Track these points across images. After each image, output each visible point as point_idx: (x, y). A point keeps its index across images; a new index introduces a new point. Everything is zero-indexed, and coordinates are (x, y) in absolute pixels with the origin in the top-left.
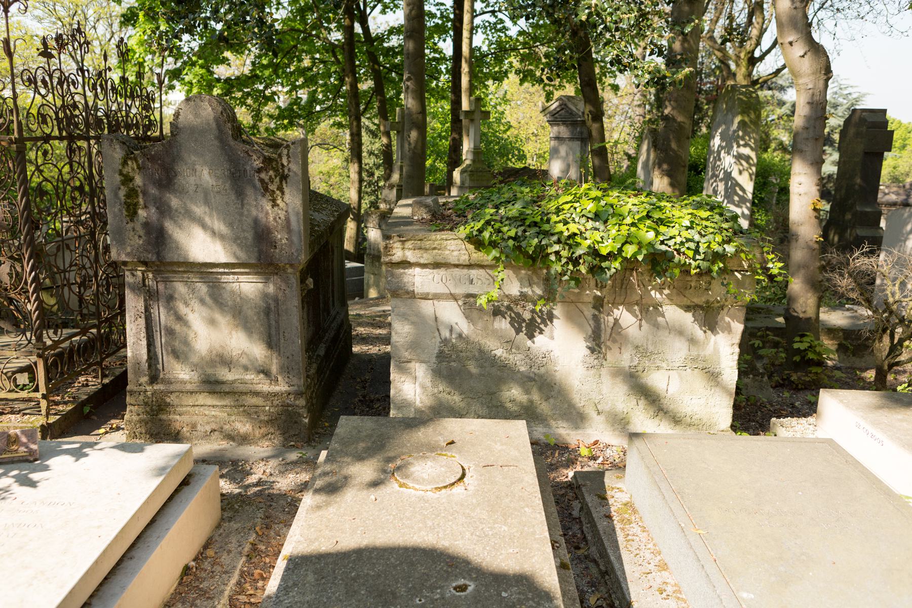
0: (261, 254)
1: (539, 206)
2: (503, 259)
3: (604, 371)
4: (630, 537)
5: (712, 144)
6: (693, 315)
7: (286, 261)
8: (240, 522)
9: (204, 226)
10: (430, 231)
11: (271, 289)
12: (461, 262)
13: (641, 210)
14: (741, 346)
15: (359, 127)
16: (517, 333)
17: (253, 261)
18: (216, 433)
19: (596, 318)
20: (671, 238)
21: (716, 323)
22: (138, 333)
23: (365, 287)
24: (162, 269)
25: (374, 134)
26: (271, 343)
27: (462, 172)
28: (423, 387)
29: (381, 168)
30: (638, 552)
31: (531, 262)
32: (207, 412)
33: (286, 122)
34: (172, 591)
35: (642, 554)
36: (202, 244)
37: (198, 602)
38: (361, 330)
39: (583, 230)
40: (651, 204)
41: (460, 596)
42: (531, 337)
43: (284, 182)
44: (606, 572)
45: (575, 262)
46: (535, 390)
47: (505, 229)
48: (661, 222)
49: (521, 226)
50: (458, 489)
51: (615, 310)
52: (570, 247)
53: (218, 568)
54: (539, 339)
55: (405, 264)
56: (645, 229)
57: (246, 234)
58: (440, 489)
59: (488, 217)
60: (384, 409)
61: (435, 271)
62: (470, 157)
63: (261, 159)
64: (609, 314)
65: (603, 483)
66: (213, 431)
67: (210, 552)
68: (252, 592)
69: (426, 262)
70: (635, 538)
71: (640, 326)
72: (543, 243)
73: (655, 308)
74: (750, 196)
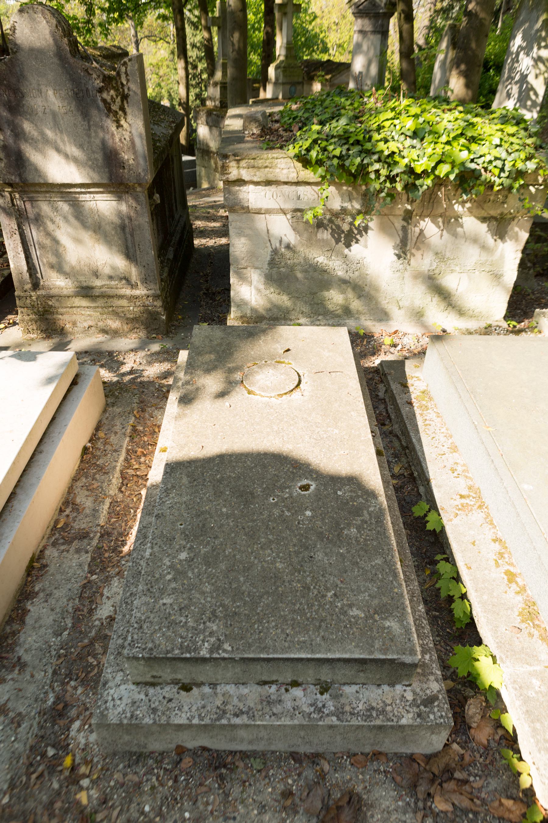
0: (112, 174)
1: (361, 122)
2: (328, 177)
3: (407, 274)
4: (427, 422)
5: (512, 44)
6: (488, 226)
7: (135, 181)
8: (121, 407)
9: (58, 150)
10: (262, 149)
11: (124, 208)
12: (290, 180)
13: (456, 127)
14: (523, 252)
15: (183, 20)
16: (337, 243)
17: (105, 181)
18: (93, 328)
19: (404, 229)
20: (481, 156)
21: (506, 232)
22: (16, 247)
23: (198, 178)
24: (26, 189)
25: (195, 26)
26: (129, 254)
27: (277, 68)
28: (259, 291)
29: (203, 61)
30: (434, 435)
31: (352, 179)
32: (83, 312)
33: (116, 15)
34: (76, 468)
35: (437, 438)
36: (59, 167)
37: (97, 476)
38: (199, 224)
39: (401, 148)
40: (465, 121)
41: (305, 495)
42: (348, 246)
43: (125, 102)
44: (407, 447)
45: (392, 179)
46: (349, 290)
47: (331, 148)
48: (473, 140)
49: (345, 144)
50: (296, 394)
51: (422, 222)
52: (389, 165)
53: (108, 447)
54: (355, 247)
55: (240, 182)
56: (459, 148)
57: (96, 156)
58: (281, 395)
59: (315, 136)
60: (224, 301)
61: (267, 188)
62: (283, 52)
63: (101, 77)
64: (416, 226)
65: (404, 372)
66: (90, 327)
67: (101, 434)
68: (137, 466)
69: (259, 180)
70: (431, 423)
71: (442, 236)
72: (365, 162)
73: (456, 220)
74: (540, 99)
